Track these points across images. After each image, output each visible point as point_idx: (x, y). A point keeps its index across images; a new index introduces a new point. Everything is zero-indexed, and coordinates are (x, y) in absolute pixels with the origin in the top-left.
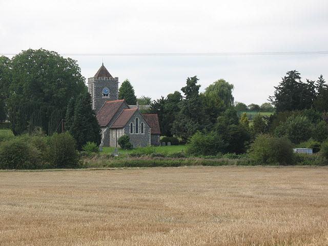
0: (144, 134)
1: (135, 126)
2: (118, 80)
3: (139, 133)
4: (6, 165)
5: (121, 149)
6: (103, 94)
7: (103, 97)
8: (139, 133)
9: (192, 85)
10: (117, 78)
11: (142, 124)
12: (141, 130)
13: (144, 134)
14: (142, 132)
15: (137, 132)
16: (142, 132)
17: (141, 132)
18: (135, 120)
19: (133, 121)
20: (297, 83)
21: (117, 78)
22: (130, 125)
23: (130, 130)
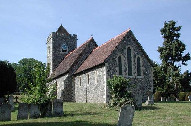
0: (141, 77)
1: (127, 61)
2: (76, 38)
3: (134, 75)
4: (62, 105)
5: (175, 22)
6: (61, 50)
7: (61, 53)
8: (134, 75)
9: (190, 55)
10: (75, 36)
11: (138, 58)
12: (136, 70)
13: (141, 77)
14: (139, 74)
15: (130, 74)
16: (139, 74)
17: (136, 74)
18: (126, 51)
19: (123, 53)
20: (42, 113)
21: (75, 36)
22: (117, 59)
23: (117, 69)
